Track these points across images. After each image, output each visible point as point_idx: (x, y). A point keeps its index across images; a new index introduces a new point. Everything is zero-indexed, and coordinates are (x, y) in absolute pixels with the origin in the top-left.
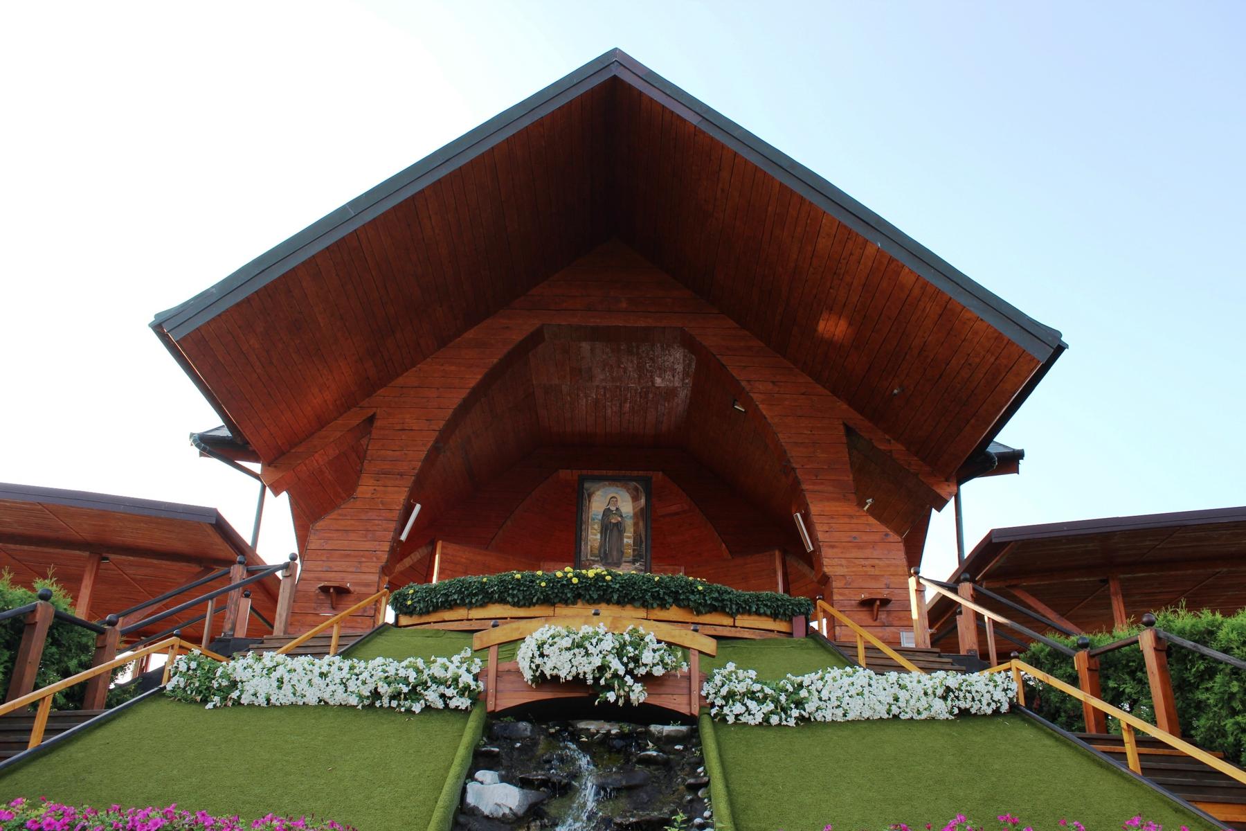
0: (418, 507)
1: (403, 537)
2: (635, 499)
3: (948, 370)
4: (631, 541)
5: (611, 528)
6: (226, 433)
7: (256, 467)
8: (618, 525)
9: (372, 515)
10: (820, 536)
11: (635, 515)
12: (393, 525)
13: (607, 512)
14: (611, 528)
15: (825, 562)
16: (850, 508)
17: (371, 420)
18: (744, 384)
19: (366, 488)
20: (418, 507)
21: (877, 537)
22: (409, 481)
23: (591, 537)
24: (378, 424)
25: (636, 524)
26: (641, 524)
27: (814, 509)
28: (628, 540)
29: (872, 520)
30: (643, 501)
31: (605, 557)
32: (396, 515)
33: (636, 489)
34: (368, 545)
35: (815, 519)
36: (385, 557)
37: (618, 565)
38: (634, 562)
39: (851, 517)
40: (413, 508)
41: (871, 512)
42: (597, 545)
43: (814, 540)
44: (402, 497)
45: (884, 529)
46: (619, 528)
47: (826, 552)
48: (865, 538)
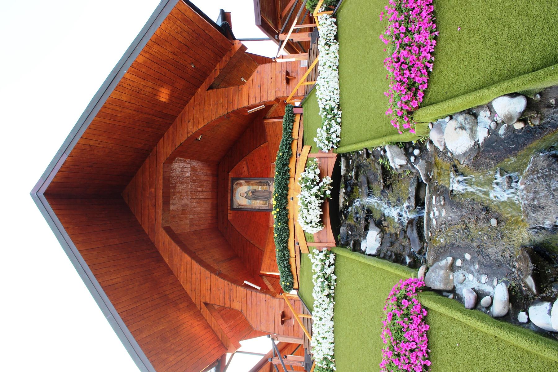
0: (246, 282)
1: (259, 288)
2: (241, 185)
4: (260, 187)
7: (228, 355)
8: (253, 193)
10: (258, 101)
11: (248, 185)
12: (254, 293)
13: (247, 198)
14: (254, 196)
15: (269, 100)
16: (246, 87)
17: (206, 304)
19: (237, 306)
20: (246, 282)
21: (259, 76)
22: (234, 286)
23: (258, 205)
24: (208, 301)
25: (252, 184)
26: (252, 182)
27: (246, 104)
28: (259, 188)
30: (242, 181)
31: (268, 199)
32: (249, 292)
33: (237, 184)
35: (250, 104)
39: (249, 88)
42: (262, 202)
44: (241, 290)
45: (254, 73)
47: (265, 99)
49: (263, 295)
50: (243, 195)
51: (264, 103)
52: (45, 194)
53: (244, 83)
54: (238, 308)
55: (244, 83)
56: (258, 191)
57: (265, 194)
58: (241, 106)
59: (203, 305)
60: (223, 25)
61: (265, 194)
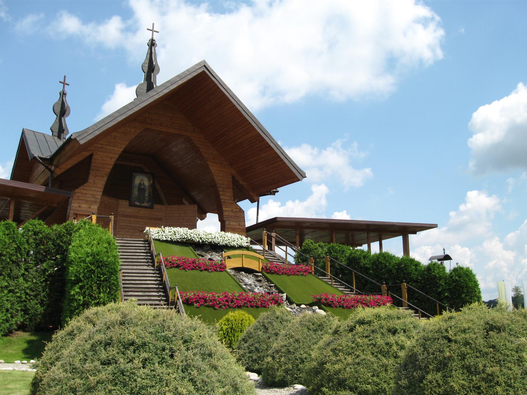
2: (149, 180)
5: (141, 189)
13: (140, 184)
19: (91, 179)
23: (135, 192)
28: (147, 194)
31: (139, 201)
37: (143, 203)
38: (148, 202)
42: (136, 195)
56: (144, 194)
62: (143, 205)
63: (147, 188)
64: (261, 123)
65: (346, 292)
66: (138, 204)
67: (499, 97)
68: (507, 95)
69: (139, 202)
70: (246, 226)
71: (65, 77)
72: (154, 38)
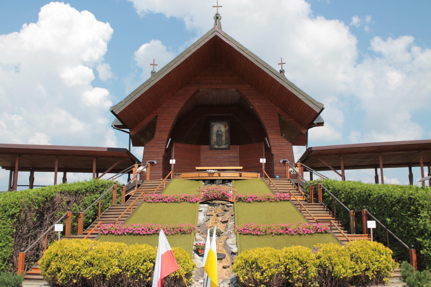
0: (170, 139)
1: (167, 147)
2: (225, 127)
3: (300, 115)
4: (224, 139)
5: (219, 135)
6: (121, 124)
7: (128, 130)
8: (221, 134)
9: (159, 142)
10: (271, 144)
11: (225, 131)
12: (165, 145)
13: (218, 131)
14: (219, 135)
15: (272, 150)
17: (157, 116)
18: (252, 103)
19: (157, 135)
20: (170, 139)
21: (286, 144)
22: (168, 133)
23: (214, 138)
24: (158, 118)
25: (226, 134)
26: (227, 134)
27: (270, 137)
28: (224, 138)
29: (284, 139)
30: (227, 128)
31: (218, 144)
32: (165, 142)
33: (226, 124)
34: (159, 150)
35: (270, 140)
36: (163, 153)
37: (221, 145)
38: (225, 144)
39: (279, 139)
40: (169, 139)
41: (284, 137)
42: (215, 140)
43: (270, 145)
44: (166, 137)
45: (287, 142)
46: (221, 135)
47: (272, 148)
48: (283, 144)
49: (164, 150)
50: (219, 129)
51: (270, 148)
52: (216, 35)
53: (282, 135)
54: (155, 136)
55: (282, 135)
56: (222, 138)
57: (220, 142)
58: (269, 134)
59: (156, 115)
60: (314, 124)
61: (220, 142)
62: (221, 147)
63: (224, 134)
64: (311, 96)
65: (213, 171)
66: (217, 147)
67: (198, 50)
68: (49, 3)
69: (218, 145)
70: (143, 147)
71: (279, 64)
72: (219, 13)
